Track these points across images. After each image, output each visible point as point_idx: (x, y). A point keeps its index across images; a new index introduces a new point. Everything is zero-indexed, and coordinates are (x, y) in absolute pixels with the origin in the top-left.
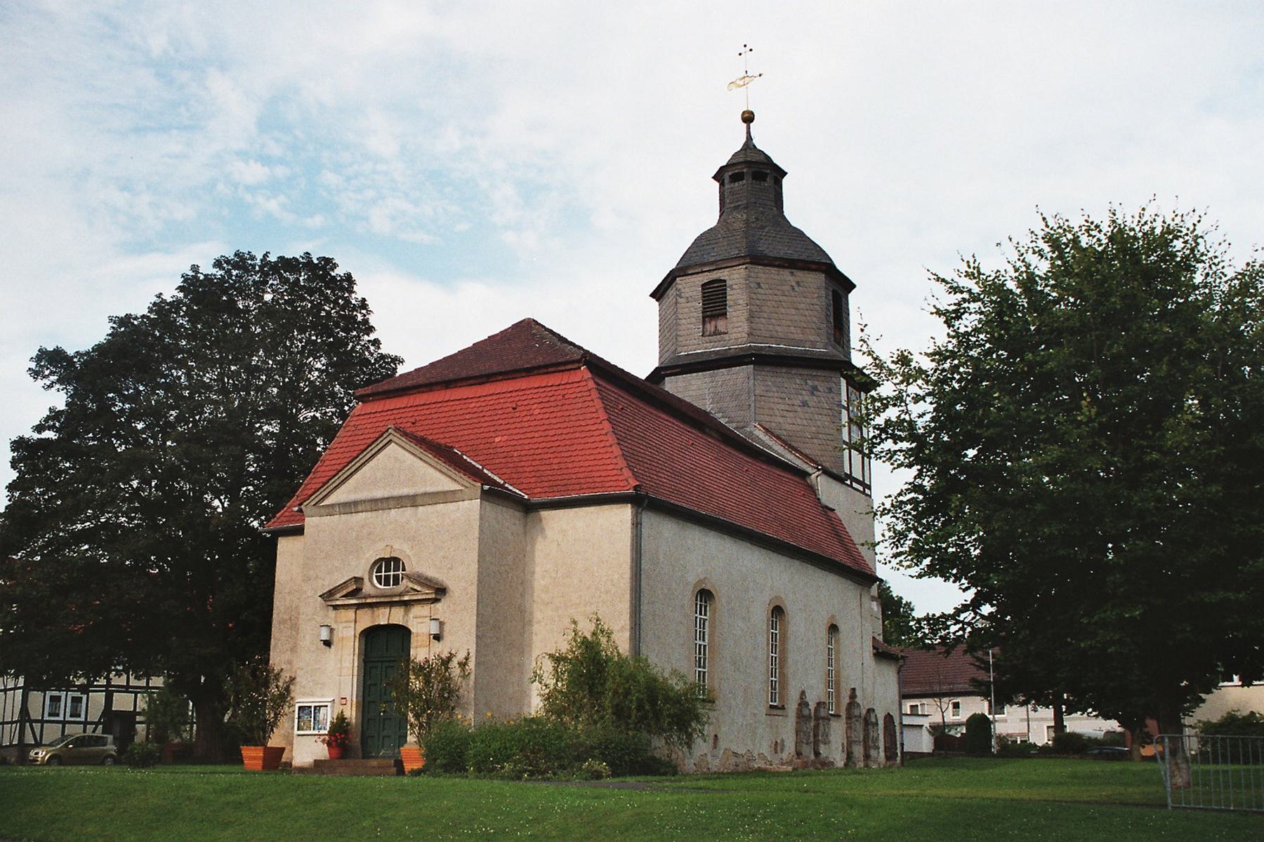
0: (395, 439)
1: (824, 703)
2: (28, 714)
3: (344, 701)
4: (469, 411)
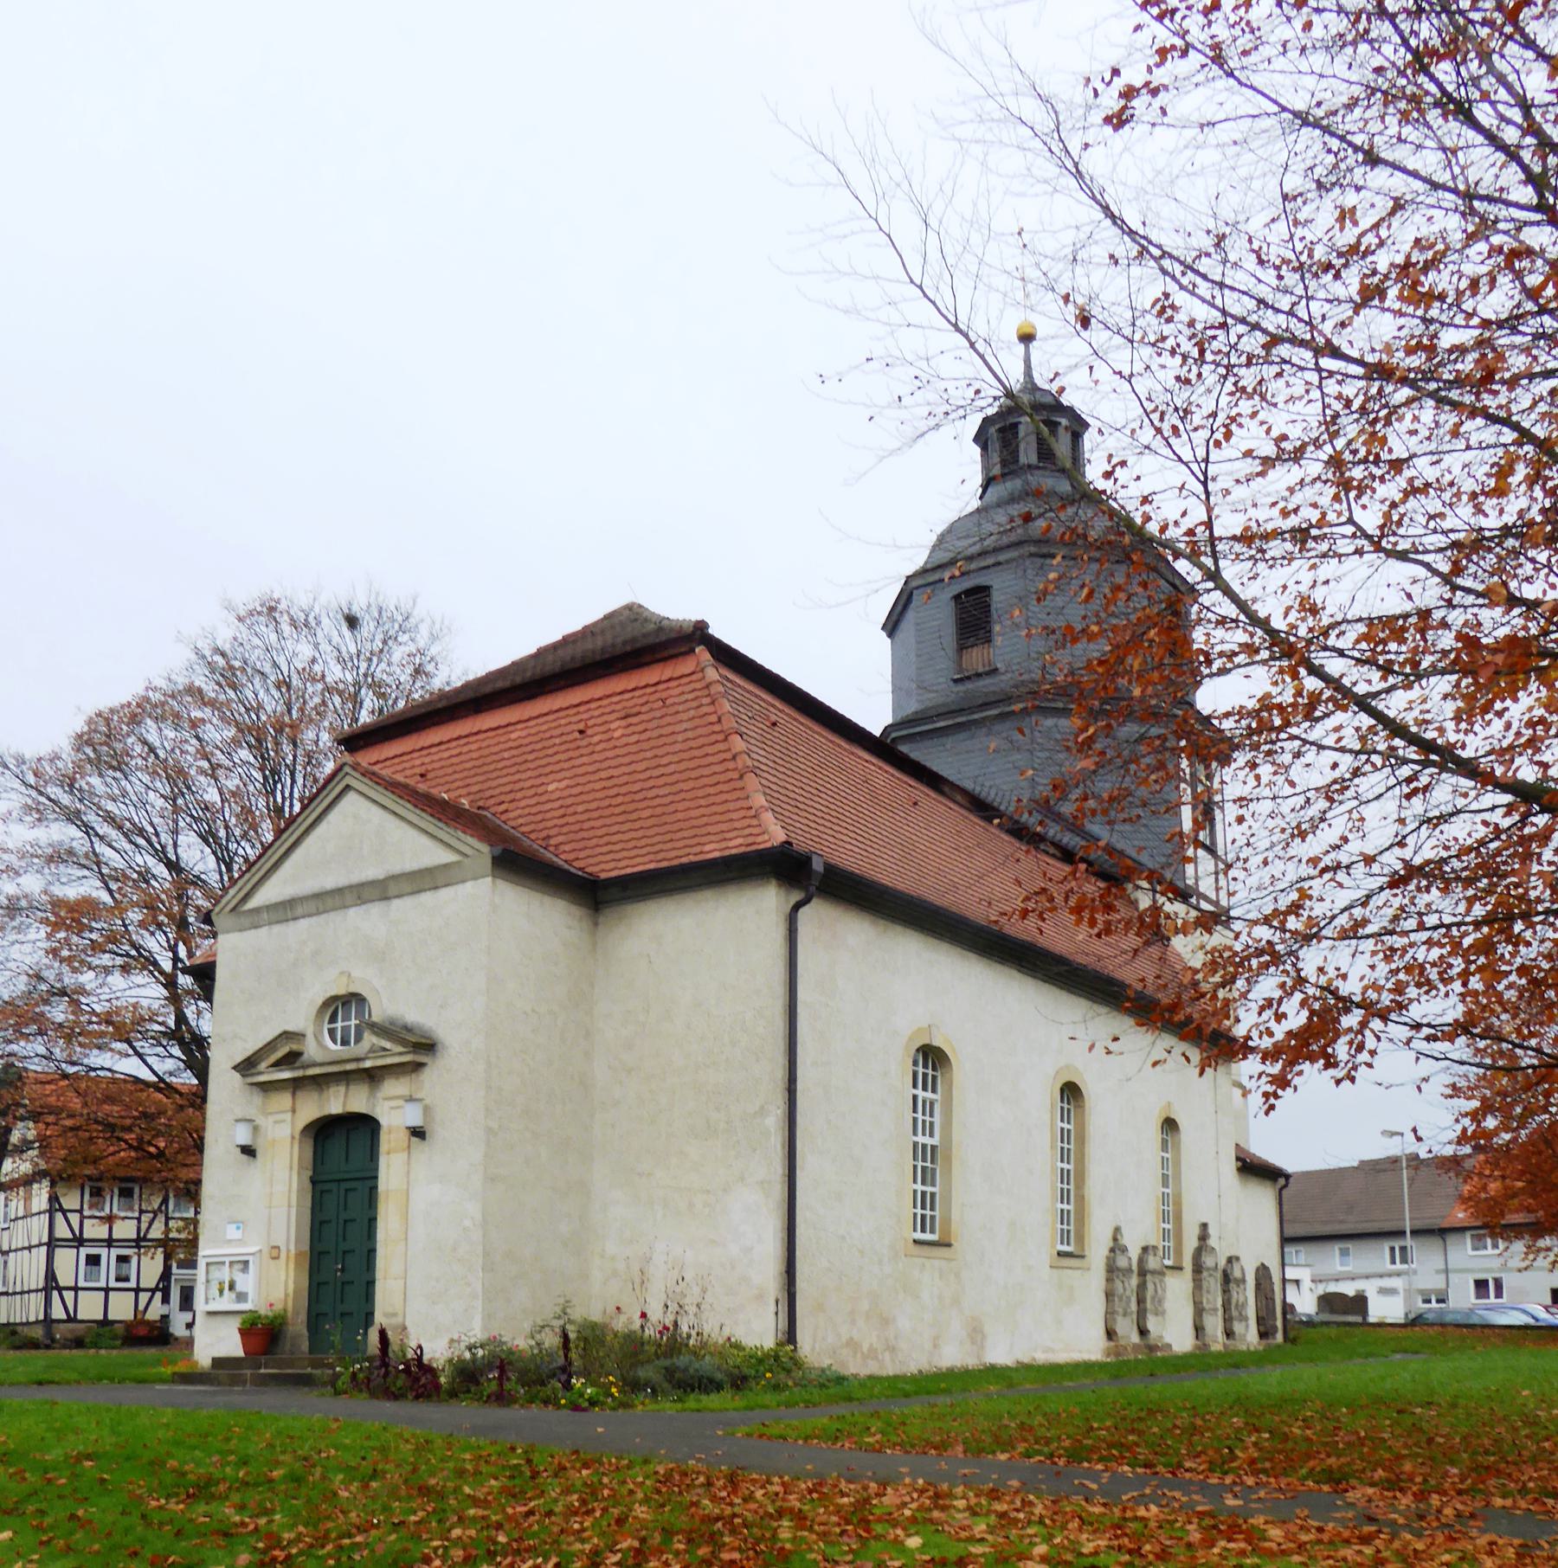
0: (354, 783)
1: (1155, 1248)
2: (54, 1278)
3: (275, 1253)
4: (511, 744)
